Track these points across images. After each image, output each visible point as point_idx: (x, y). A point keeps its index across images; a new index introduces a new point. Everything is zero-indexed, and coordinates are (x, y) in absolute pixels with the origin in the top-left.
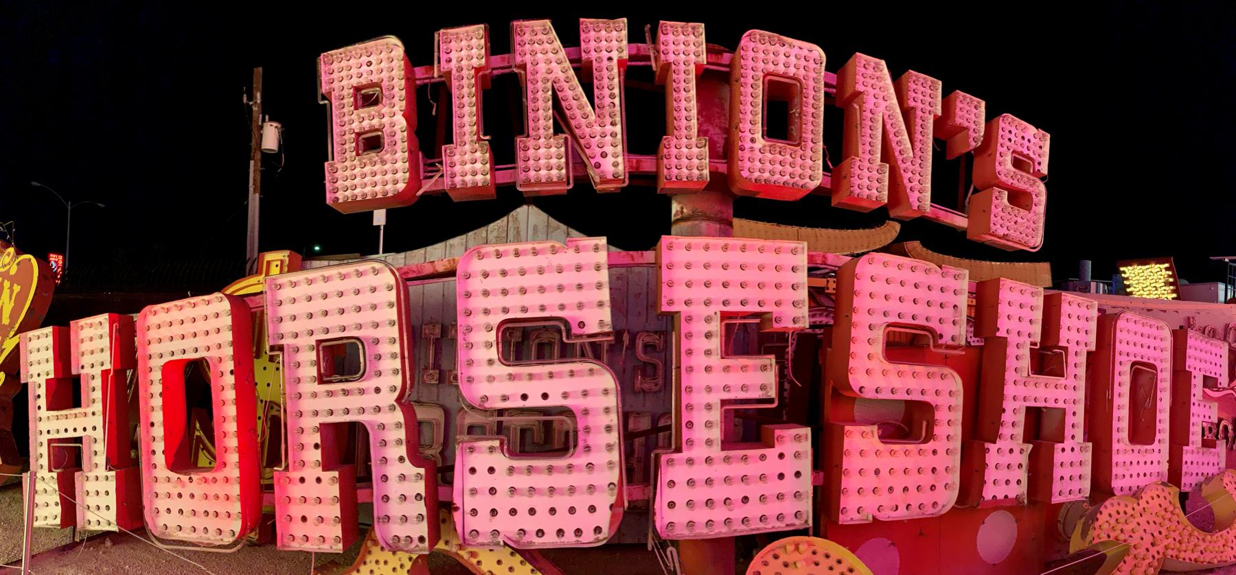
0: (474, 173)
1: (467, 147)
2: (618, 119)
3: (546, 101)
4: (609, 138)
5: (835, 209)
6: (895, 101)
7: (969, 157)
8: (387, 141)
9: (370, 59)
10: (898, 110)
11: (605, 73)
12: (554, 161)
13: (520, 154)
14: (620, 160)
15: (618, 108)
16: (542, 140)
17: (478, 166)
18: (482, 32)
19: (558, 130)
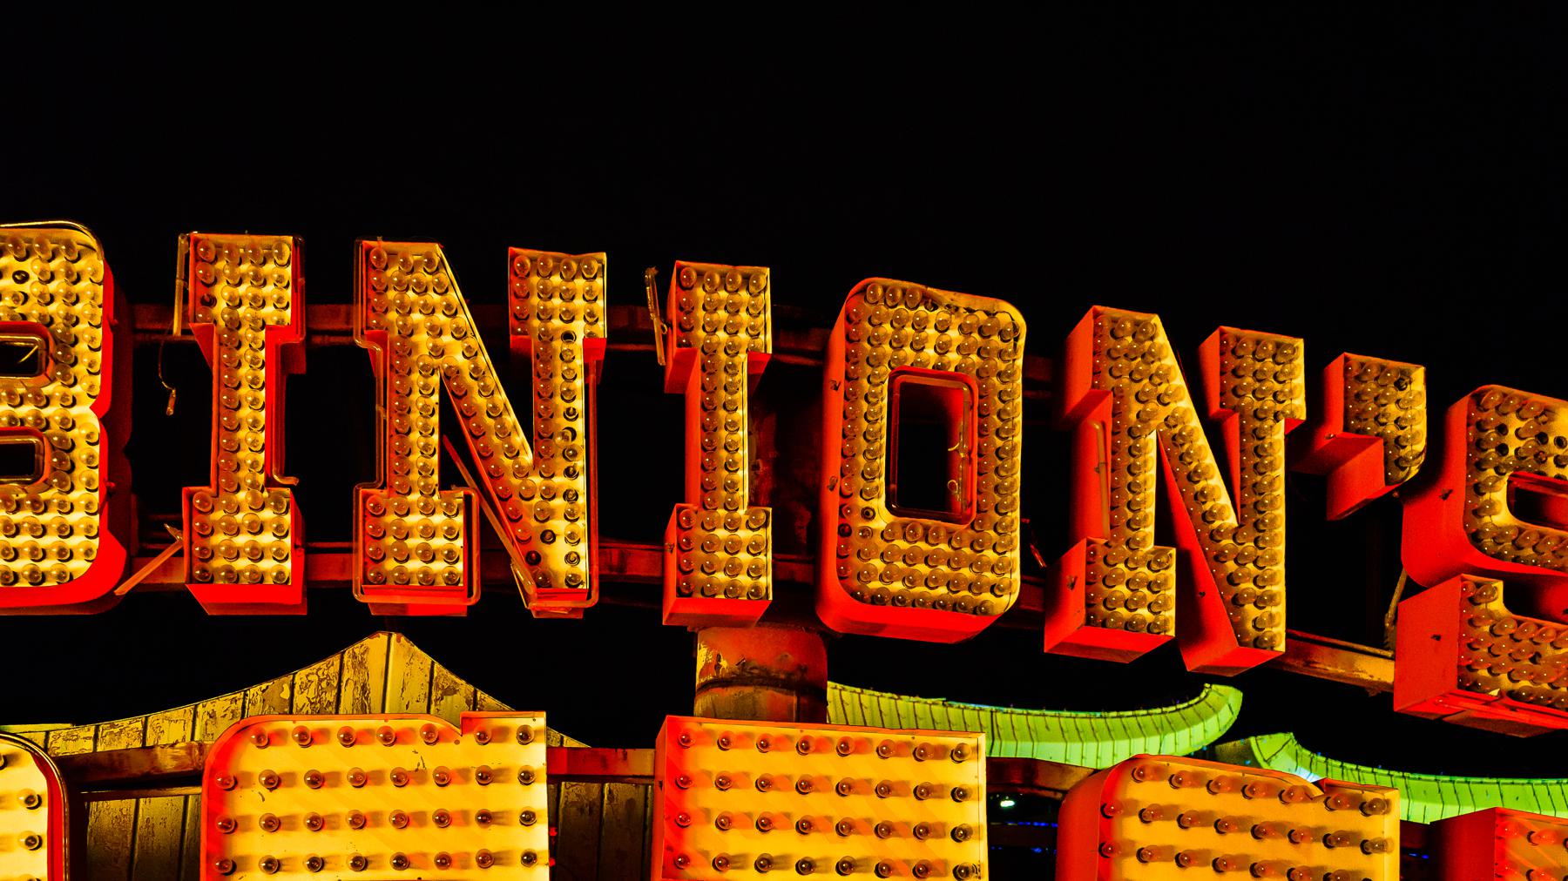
0: (257, 554)
1: (242, 496)
2: (580, 463)
3: (426, 412)
4: (559, 502)
5: (1051, 657)
6: (1185, 403)
7: (1384, 514)
8: (50, 460)
9: (25, 266)
10: (1194, 422)
11: (560, 367)
12: (439, 542)
13: (364, 527)
14: (582, 549)
15: (580, 441)
16: (414, 497)
17: (266, 539)
18: (287, 252)
19: (449, 479)
